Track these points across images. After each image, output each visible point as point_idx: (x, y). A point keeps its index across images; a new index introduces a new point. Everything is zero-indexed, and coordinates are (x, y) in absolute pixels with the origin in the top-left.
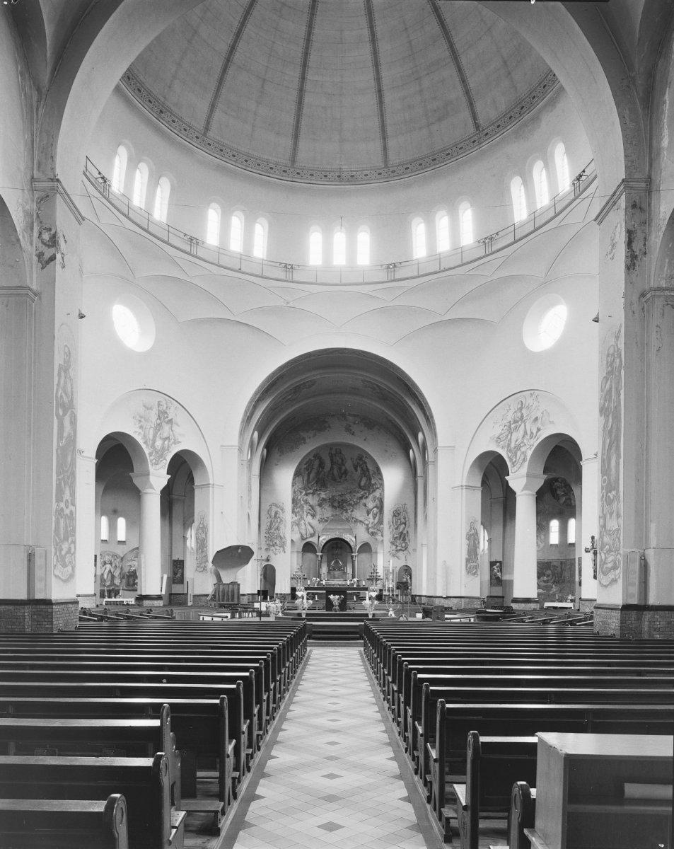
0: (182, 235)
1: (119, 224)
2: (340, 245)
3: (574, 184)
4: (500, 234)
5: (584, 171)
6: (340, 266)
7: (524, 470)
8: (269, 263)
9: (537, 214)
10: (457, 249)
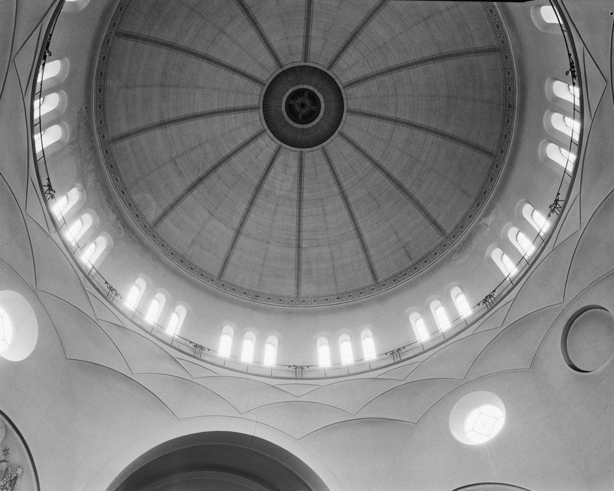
2: (247, 347)
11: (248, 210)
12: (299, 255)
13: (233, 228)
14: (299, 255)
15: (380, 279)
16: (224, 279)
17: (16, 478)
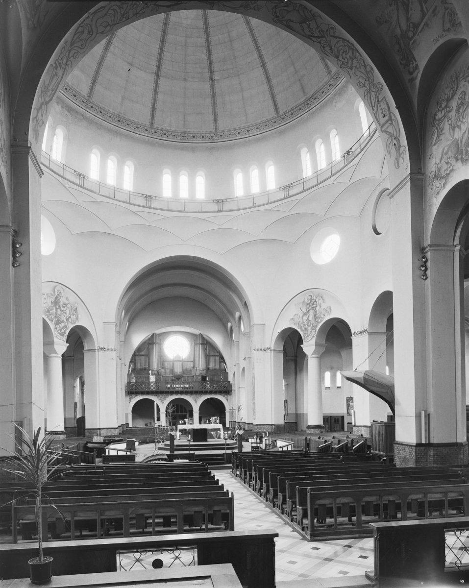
0: (73, 171)
1: (161, 217)
2: (184, 184)
3: (344, 156)
4: (294, 184)
5: (351, 149)
6: (188, 199)
7: (313, 341)
8: (134, 194)
9: (319, 173)
10: (265, 193)
11: (161, 49)
12: (213, 88)
13: (152, 73)
14: (213, 88)
15: (281, 113)
16: (155, 125)
17: (76, 308)
